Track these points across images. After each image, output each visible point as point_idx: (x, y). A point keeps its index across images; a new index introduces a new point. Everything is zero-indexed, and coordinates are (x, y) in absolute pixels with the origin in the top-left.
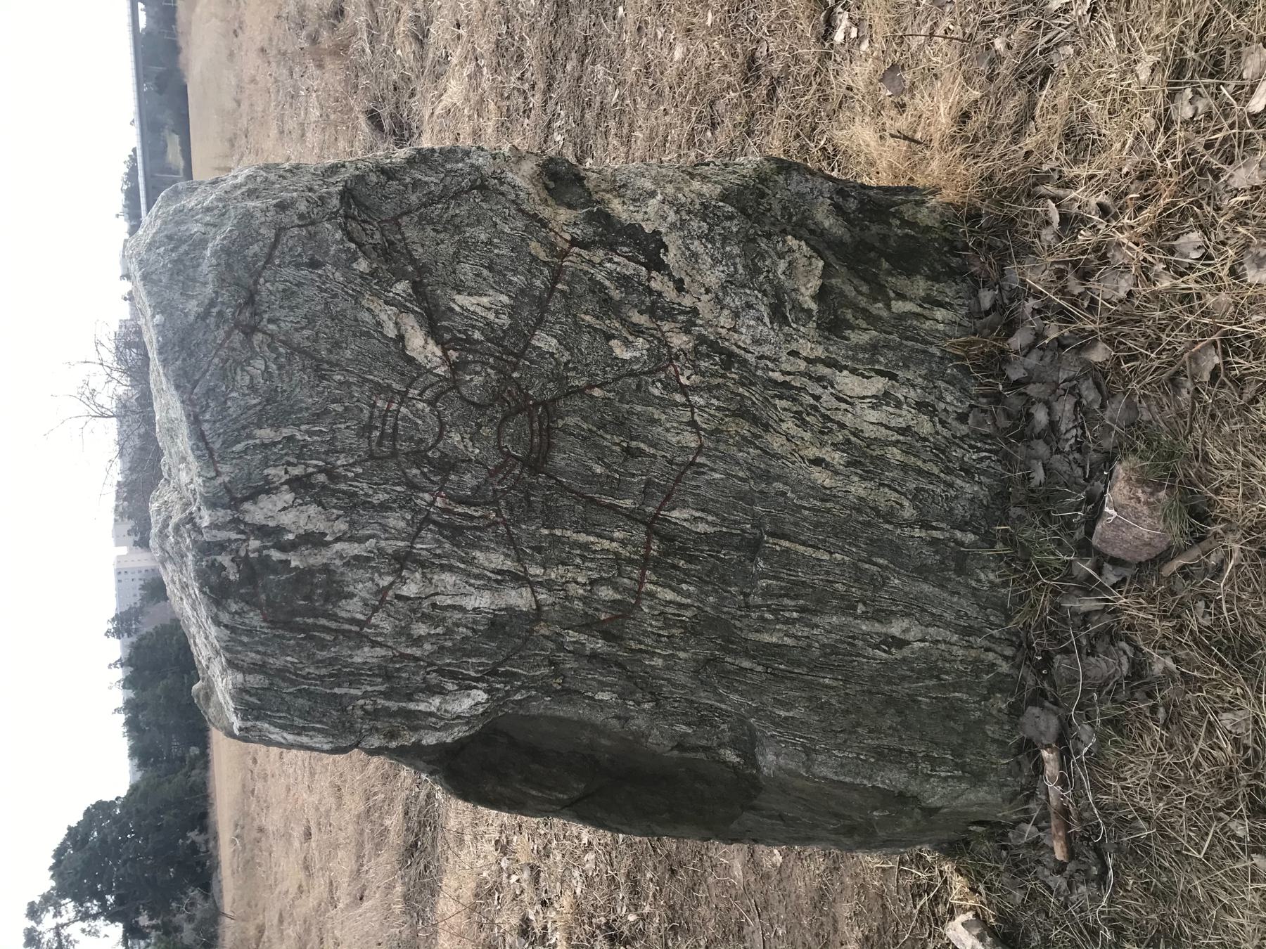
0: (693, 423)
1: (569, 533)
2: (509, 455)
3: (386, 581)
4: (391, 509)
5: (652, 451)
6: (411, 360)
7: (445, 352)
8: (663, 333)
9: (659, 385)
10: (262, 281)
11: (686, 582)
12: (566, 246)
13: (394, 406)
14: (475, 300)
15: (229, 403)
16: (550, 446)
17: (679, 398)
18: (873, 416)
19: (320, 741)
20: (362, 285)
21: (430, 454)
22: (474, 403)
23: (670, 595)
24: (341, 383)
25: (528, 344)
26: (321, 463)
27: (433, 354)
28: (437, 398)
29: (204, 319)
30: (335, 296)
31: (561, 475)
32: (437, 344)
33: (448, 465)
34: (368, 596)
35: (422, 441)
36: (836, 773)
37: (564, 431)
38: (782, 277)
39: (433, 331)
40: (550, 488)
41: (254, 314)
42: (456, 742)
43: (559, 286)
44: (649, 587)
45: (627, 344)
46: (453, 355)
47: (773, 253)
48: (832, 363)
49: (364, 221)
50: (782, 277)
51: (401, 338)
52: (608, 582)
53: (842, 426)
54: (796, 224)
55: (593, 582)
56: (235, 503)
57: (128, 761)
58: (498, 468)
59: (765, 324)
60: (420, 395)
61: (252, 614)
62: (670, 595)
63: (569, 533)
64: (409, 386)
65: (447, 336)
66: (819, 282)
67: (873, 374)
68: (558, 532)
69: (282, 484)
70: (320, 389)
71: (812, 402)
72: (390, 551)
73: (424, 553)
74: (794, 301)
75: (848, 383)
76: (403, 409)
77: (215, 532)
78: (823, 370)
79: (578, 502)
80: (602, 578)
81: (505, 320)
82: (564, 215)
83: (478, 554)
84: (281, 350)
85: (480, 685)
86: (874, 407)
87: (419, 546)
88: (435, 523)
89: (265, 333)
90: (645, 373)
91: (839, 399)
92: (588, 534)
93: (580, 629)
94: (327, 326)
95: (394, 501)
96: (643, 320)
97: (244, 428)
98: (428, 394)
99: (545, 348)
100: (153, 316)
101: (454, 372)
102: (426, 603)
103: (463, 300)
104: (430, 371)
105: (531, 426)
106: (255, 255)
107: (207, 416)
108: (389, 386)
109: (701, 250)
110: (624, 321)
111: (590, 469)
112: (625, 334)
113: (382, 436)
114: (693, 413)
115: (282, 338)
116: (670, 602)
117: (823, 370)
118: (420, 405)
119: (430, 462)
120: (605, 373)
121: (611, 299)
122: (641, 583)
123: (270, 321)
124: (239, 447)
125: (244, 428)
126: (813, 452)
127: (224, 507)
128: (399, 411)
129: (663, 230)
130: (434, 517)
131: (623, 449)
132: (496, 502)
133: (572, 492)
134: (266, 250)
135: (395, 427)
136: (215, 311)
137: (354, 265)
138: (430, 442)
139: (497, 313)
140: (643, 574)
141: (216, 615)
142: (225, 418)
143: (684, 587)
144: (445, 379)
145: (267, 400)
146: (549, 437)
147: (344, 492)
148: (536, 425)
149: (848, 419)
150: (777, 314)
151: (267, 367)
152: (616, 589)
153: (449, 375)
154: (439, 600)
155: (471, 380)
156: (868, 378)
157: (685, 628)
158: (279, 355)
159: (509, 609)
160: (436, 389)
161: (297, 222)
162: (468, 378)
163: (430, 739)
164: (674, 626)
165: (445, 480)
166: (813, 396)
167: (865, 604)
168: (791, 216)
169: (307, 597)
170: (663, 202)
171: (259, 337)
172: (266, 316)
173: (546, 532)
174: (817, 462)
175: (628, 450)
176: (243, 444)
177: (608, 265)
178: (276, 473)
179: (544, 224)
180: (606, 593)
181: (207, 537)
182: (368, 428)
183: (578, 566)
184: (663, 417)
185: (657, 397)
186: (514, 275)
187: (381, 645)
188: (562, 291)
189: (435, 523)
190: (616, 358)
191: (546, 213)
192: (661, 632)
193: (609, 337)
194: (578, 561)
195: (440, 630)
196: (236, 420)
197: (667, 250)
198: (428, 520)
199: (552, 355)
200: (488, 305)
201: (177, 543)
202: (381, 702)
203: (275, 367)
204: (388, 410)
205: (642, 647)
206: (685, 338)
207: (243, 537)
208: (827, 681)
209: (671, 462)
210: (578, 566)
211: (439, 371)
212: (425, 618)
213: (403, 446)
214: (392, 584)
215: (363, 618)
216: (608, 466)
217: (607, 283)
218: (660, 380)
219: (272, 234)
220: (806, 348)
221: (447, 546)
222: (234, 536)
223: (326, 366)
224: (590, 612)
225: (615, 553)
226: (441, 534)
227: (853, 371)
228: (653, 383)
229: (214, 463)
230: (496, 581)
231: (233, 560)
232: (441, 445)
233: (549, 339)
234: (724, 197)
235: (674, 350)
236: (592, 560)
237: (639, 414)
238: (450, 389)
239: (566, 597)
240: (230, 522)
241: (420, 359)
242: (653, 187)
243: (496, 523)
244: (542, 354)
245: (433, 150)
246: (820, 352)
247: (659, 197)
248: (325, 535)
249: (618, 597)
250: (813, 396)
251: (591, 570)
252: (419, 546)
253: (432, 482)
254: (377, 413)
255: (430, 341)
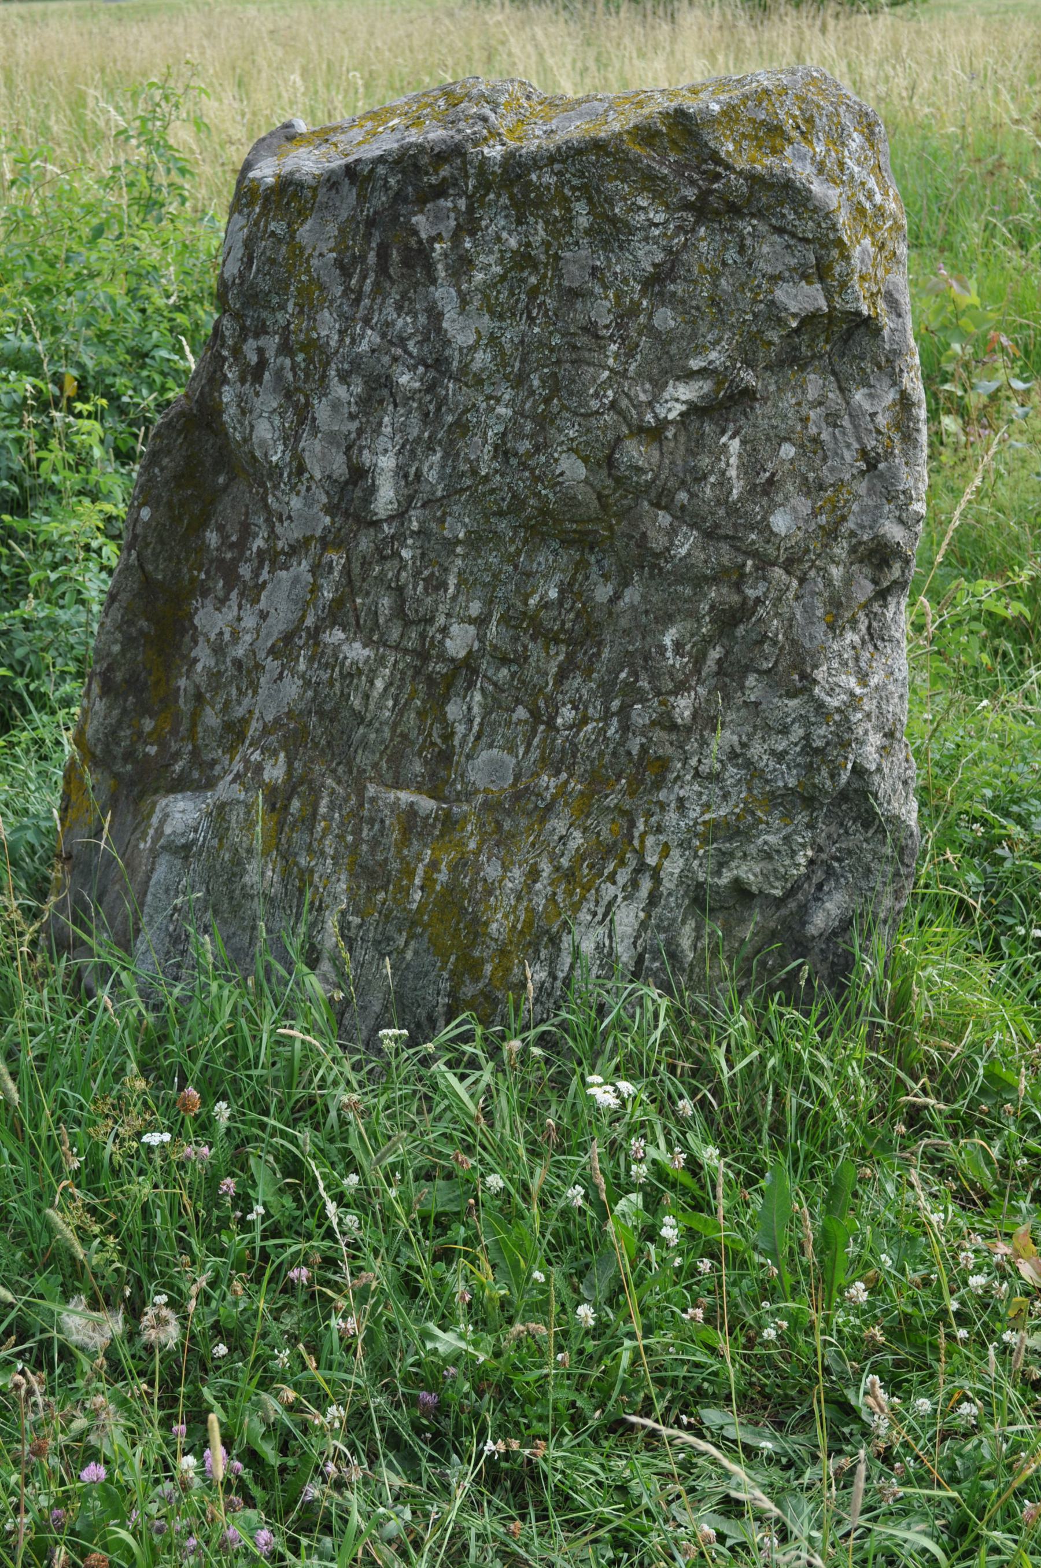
0: (585, 720)
10: (755, 222)
17: (615, 705)
18: (588, 947)
19: (233, 269)
22: (613, 453)
27: (670, 410)
28: (620, 413)
32: (681, 414)
36: (158, 882)
38: (760, 841)
39: (694, 411)
41: (717, 213)
47: (789, 829)
48: (653, 899)
50: (760, 841)
53: (576, 907)
54: (830, 867)
55: (400, 590)
57: (217, 136)
59: (703, 813)
66: (754, 889)
67: (640, 949)
71: (606, 872)
72: (447, 353)
74: (732, 855)
75: (627, 918)
76: (607, 373)
78: (646, 885)
80: (404, 602)
85: (288, 454)
86: (599, 947)
91: (610, 904)
92: (458, 586)
96: (711, 664)
100: (718, 102)
102: (385, 392)
109: (793, 738)
110: (708, 642)
114: (597, 721)
117: (646, 885)
126: (546, 868)
149: (584, 916)
150: (713, 832)
151: (656, 225)
156: (635, 943)
159: (373, 490)
163: (227, 395)
166: (614, 873)
167: (360, 926)
168: (839, 860)
170: (852, 694)
174: (534, 874)
187: (341, 341)
188: (744, 565)
201: (467, 117)
206: (687, 713)
208: (270, 873)
214: (410, 355)
220: (674, 866)
225: (433, 618)
227: (644, 925)
234: (859, 771)
235: (672, 699)
237: (598, 654)
246: (668, 884)
247: (858, 691)
250: (614, 873)
255: (684, 408)
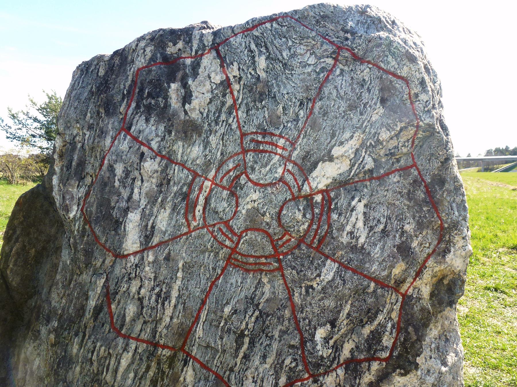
1: (179, 283)
2: (240, 237)
3: (154, 145)
4: (205, 148)
5: (241, 355)
6: (315, 166)
7: (321, 192)
8: (335, 369)
9: (293, 365)
10: (370, 66)
11: (135, 376)
12: (402, 291)
13: (279, 151)
14: (361, 217)
15: (284, 40)
16: (248, 271)
20: (370, 133)
21: (244, 176)
23: (124, 363)
24: (297, 115)
25: (327, 257)
26: (240, 100)
29: (342, 30)
30: (361, 114)
31: (224, 279)
33: (234, 190)
34: (146, 133)
35: (253, 169)
37: (259, 283)
40: (214, 269)
42: (53, 198)
43: (373, 285)
44: (133, 346)
45: (326, 340)
46: (318, 198)
49: (413, 142)
51: (331, 159)
52: (139, 314)
55: (141, 300)
56: (215, 47)
58: (231, 229)
60: (288, 170)
61: (143, 61)
62: (124, 363)
63: (179, 283)
64: (295, 163)
65: (332, 194)
68: (180, 275)
69: (227, 75)
70: (294, 100)
72: (175, 148)
73: (172, 172)
76: (278, 157)
77: (198, 37)
79: (202, 291)
81: (345, 239)
82: (426, 291)
83: (168, 211)
84: (322, 75)
85: (79, 212)
87: (177, 168)
88: (193, 180)
89: (334, 66)
90: (303, 353)
93: (106, 286)
94: (339, 108)
95: (210, 151)
97: (267, 48)
98: (289, 178)
99: (324, 270)
101: (306, 197)
103: (360, 208)
104: (307, 179)
105: (262, 257)
106: (388, 63)
107: (274, 25)
108: (295, 149)
111: (228, 303)
112: (336, 337)
113: (258, 142)
115: (331, 77)
116: (119, 363)
118: (280, 170)
119: (238, 177)
120: (304, 319)
121: (363, 326)
122: (137, 339)
123: (342, 71)
124: (253, 46)
125: (267, 48)
127: (214, 40)
128: (276, 154)
129: (419, 373)
130: (197, 179)
131: (242, 331)
132: (205, 226)
133: (211, 288)
134: (392, 70)
135: (263, 151)
136: (349, 36)
137: (384, 129)
138: (252, 176)
139: (351, 233)
140: (143, 341)
141: (144, 39)
142: (274, 36)
143: (132, 375)
144: (300, 190)
145: (286, 64)
146: (255, 271)
147: (219, 116)
148: (263, 260)
151: (309, 65)
152: (134, 320)
153: (303, 193)
154: (138, 183)
155: (299, 210)
157: (98, 374)
158: (318, 74)
160: (292, 182)
161: (413, 92)
162: (301, 208)
164: (100, 365)
165: (224, 188)
169: (150, 95)
171: (330, 61)
172: (346, 68)
173: (180, 265)
175: (242, 335)
176: (256, 49)
177: (390, 325)
178: (234, 71)
179: (419, 274)
180: (131, 310)
181: (196, 33)
182: (264, 133)
183: (153, 289)
184: (267, 366)
185: (283, 362)
186: (380, 248)
189: (193, 180)
190: (315, 329)
191: (427, 275)
192: (95, 354)
193: (333, 326)
194: (157, 290)
195: (117, 184)
196: (272, 43)
197: (402, 375)
198: (196, 175)
199: (319, 275)
200: (357, 226)
202: (79, 145)
203: (309, 70)
204: (277, 146)
205: (87, 337)
207: (193, 54)
209: (231, 370)
210: (153, 289)
211: (306, 187)
212: (127, 173)
213: (250, 157)
215: (132, 131)
216: (230, 317)
217: (376, 323)
218: (297, 365)
219: (404, 74)
221: (175, 188)
222: (195, 46)
223: (310, 105)
224: (118, 297)
226: (184, 184)
228: (295, 360)
229: (243, 32)
230: (147, 226)
231: (179, 50)
232: (250, 184)
233: (332, 274)
236: (157, 301)
238: (292, 194)
239: (130, 279)
240: (204, 44)
241: (314, 174)
242: (449, 364)
243: (189, 225)
244: (319, 267)
245: (463, 195)
248: (190, 103)
249: (128, 319)
251: (150, 299)
252: (177, 168)
253: (223, 178)
254: (275, 138)
